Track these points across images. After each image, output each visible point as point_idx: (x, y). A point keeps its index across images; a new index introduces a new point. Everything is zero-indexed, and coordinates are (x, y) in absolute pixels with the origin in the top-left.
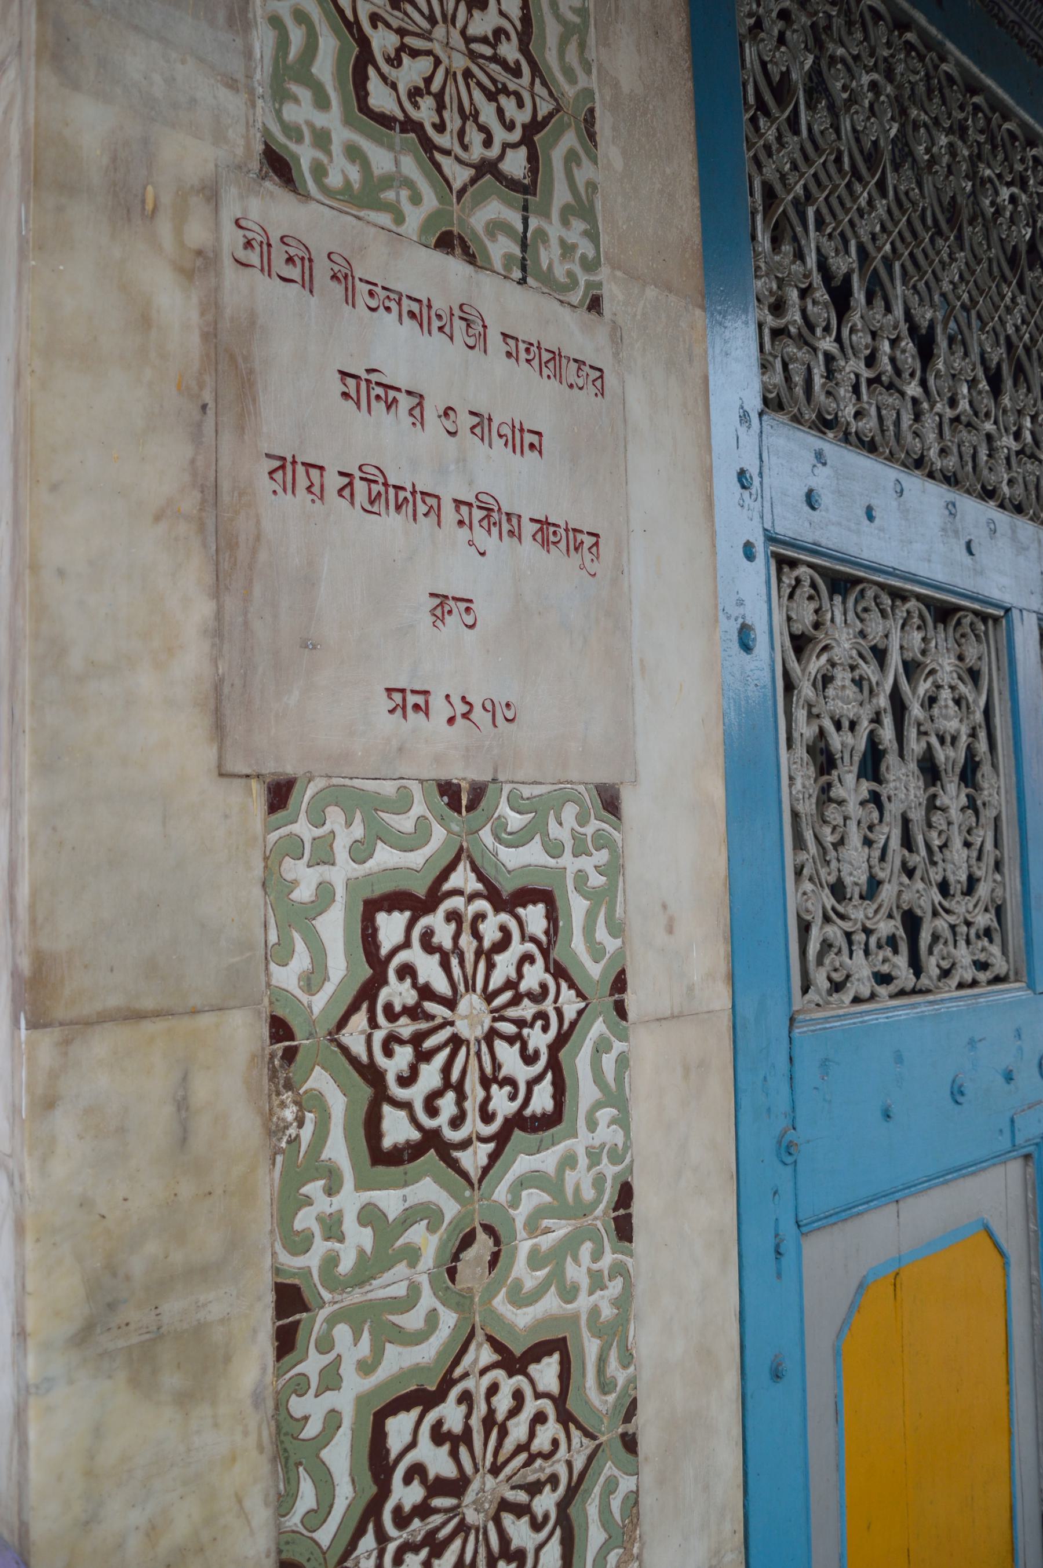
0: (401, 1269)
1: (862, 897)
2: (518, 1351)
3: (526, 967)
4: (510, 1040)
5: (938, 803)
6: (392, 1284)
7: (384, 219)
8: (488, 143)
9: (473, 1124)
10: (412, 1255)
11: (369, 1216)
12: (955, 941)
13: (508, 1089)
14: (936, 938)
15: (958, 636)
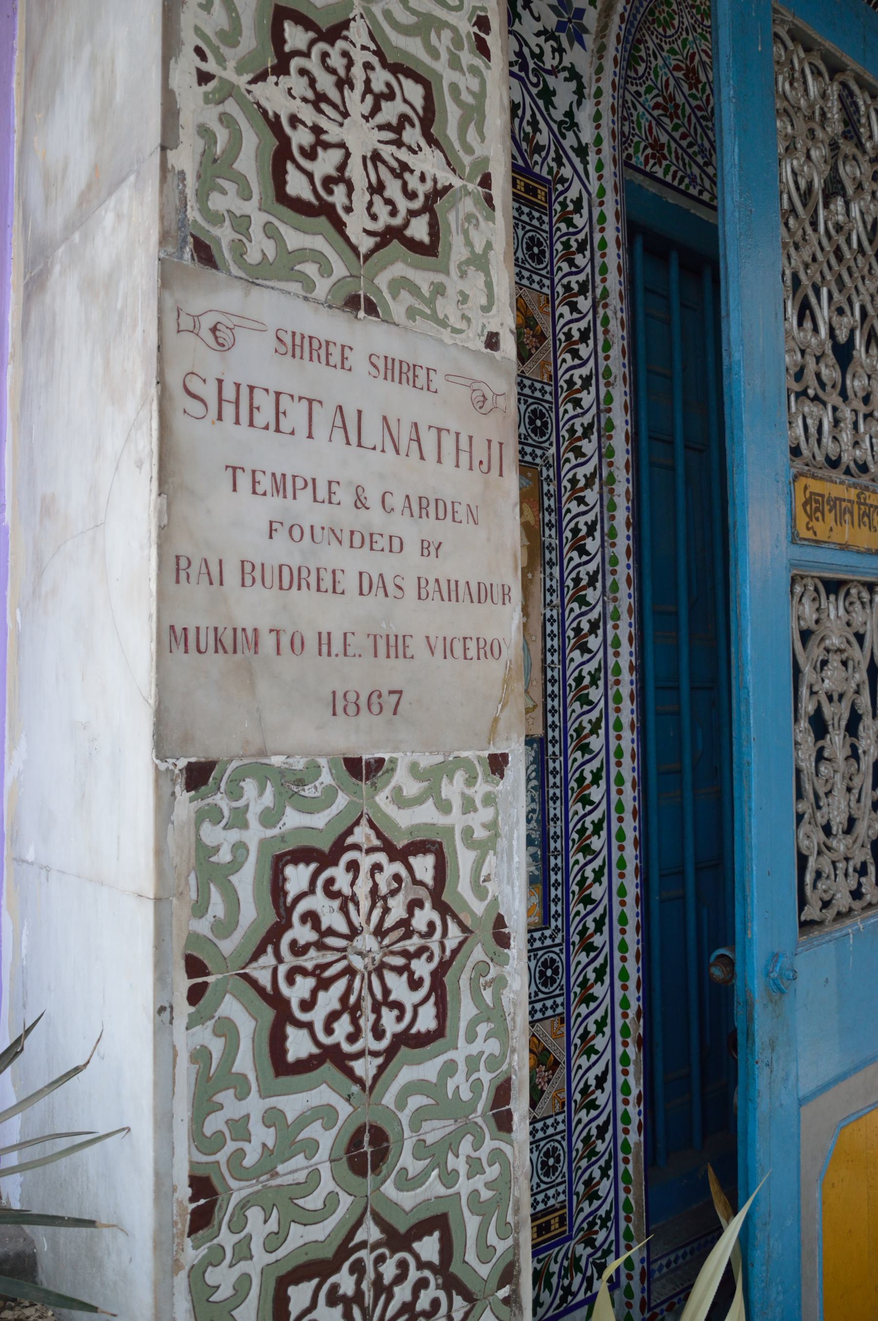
0: (299, 1160)
1: (844, 833)
2: (402, 1228)
3: (417, 911)
4: (399, 970)
5: (826, 754)
6: (293, 1169)
7: (295, 287)
8: (394, 213)
9: (367, 1041)
10: (311, 1148)
11: (273, 1118)
12: (836, 875)
13: (396, 1012)
14: (818, 875)
15: (847, 604)
